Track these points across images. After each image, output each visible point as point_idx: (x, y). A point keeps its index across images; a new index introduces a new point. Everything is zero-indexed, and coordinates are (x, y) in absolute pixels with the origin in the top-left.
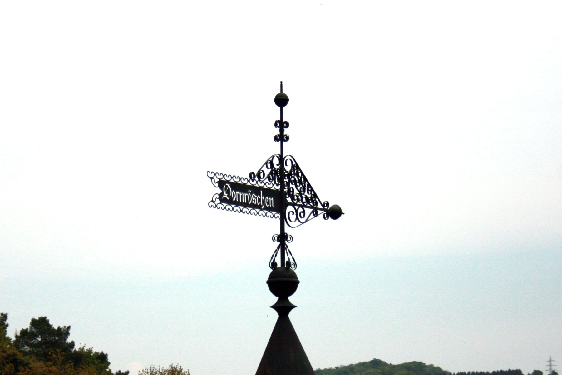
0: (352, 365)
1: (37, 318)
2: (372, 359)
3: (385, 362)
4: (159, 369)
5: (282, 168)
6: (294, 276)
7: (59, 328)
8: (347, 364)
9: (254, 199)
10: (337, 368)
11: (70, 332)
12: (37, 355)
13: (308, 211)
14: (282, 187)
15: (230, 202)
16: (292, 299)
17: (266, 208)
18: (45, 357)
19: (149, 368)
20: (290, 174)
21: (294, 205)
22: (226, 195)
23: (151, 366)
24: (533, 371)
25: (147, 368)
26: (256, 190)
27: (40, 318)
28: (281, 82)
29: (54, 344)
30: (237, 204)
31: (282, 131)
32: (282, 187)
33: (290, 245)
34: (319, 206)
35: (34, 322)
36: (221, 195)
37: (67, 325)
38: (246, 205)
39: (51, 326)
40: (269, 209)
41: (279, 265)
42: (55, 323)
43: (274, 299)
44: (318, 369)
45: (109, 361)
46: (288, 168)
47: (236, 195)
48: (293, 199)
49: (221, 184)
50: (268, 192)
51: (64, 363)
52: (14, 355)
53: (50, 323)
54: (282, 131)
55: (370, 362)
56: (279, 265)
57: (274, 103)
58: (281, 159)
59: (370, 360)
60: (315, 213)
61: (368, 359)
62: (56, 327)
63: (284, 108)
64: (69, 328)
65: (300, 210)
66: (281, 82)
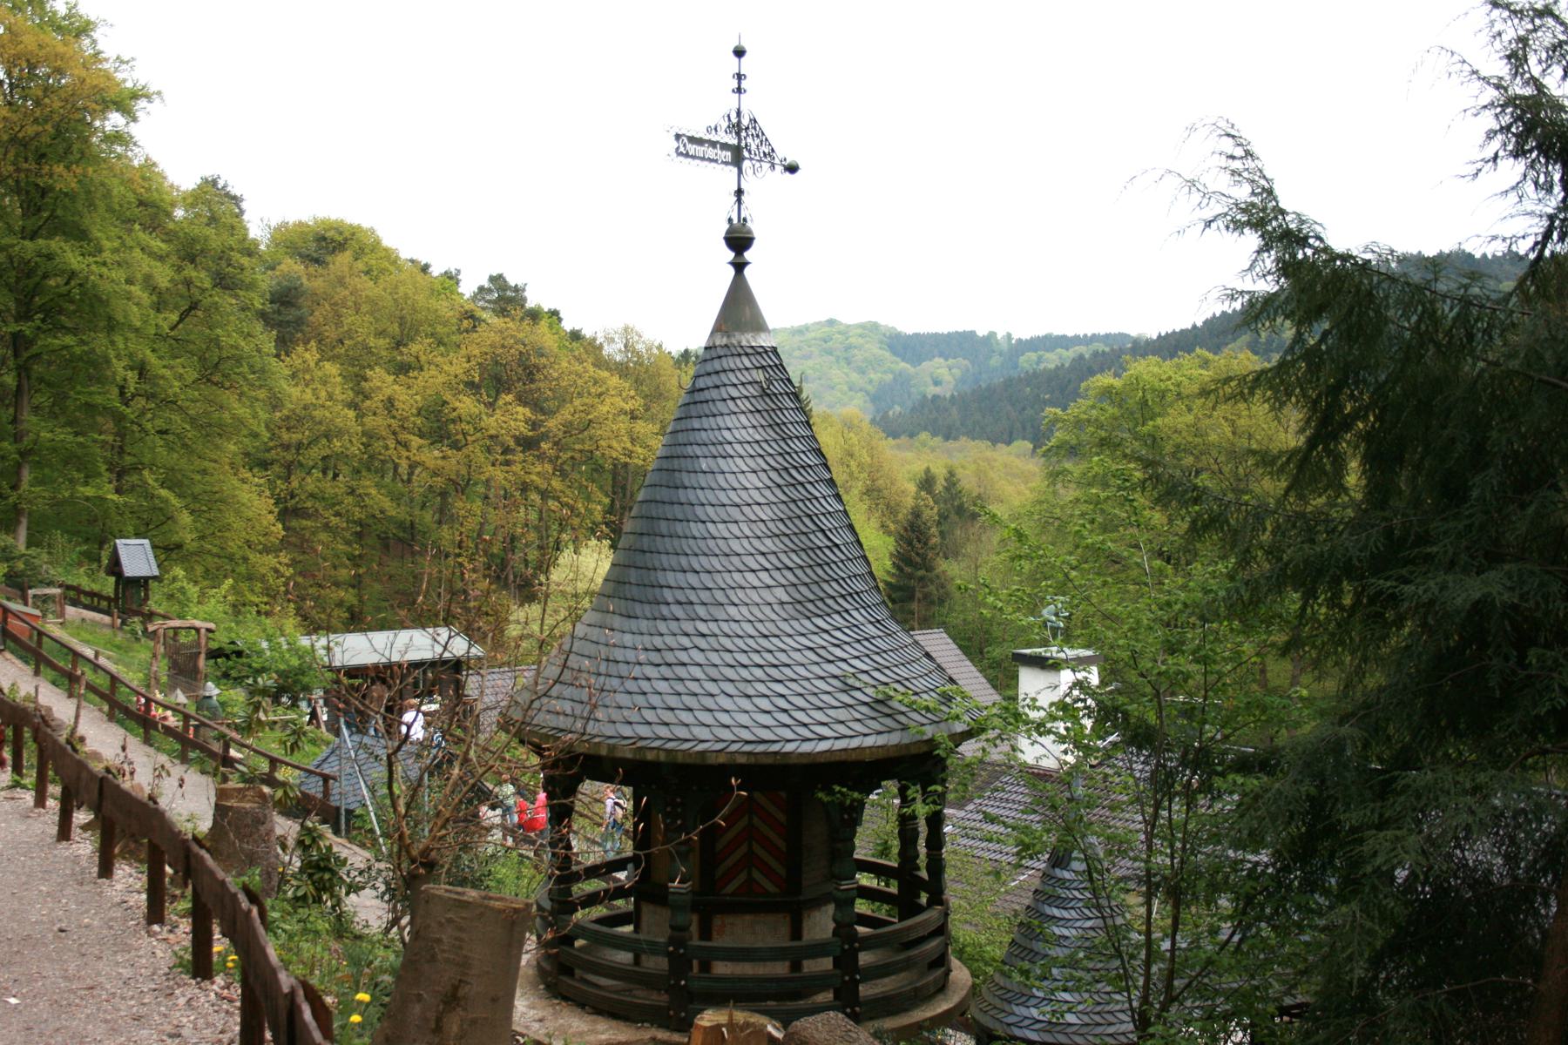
0: (973, 333)
5: (739, 122)
6: (750, 232)
9: (711, 153)
12: (494, 310)
13: (766, 166)
14: (740, 140)
15: (687, 155)
16: (748, 255)
17: (723, 162)
18: (502, 312)
20: (747, 128)
21: (751, 159)
22: (682, 149)
24: (986, 334)
26: (713, 144)
29: (510, 300)
30: (693, 157)
31: (739, 84)
32: (740, 140)
33: (743, 198)
34: (777, 161)
35: (492, 279)
36: (678, 148)
38: (703, 159)
40: (726, 163)
41: (735, 221)
42: (512, 281)
43: (731, 255)
45: (1190, 327)
46: (745, 122)
47: (692, 148)
48: (750, 152)
49: (678, 137)
50: (725, 146)
51: (522, 319)
52: (472, 311)
54: (739, 84)
56: (735, 221)
57: (723, 242)
58: (739, 113)
60: (773, 166)
61: (824, 318)
63: (727, 226)
65: (758, 165)
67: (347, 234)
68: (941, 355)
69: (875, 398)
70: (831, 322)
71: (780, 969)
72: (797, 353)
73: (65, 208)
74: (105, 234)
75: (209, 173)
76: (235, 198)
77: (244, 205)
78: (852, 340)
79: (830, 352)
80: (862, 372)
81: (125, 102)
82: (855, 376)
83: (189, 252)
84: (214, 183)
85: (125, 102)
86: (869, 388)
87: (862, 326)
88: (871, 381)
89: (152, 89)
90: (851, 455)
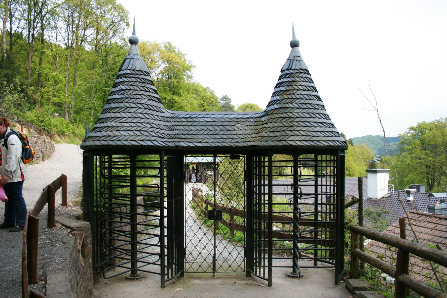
61: (368, 135)
67: (251, 106)
68: (393, 141)
69: (379, 151)
70: (370, 135)
71: (262, 192)
72: (363, 142)
73: (177, 89)
74: (185, 95)
75: (224, 95)
76: (229, 99)
77: (231, 100)
78: (374, 139)
79: (369, 141)
80: (376, 145)
81: (189, 68)
82: (375, 146)
83: (204, 98)
84: (225, 96)
85: (189, 68)
86: (378, 148)
87: (376, 136)
88: (378, 147)
89: (194, 65)
90: (363, 153)
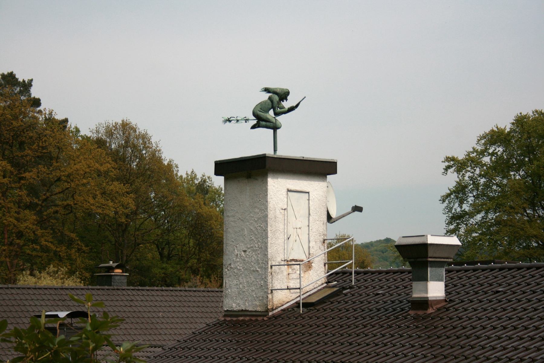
0: (372, 242)
1: (6, 73)
2: (385, 238)
3: (394, 240)
4: (112, 123)
7: (24, 81)
8: (368, 241)
10: (362, 244)
11: (32, 83)
19: (105, 123)
23: (106, 121)
25: (102, 123)
27: (8, 73)
28: (305, 97)
37: (30, 79)
39: (17, 79)
42: (21, 77)
44: (275, 174)
53: (17, 77)
55: (384, 240)
59: (384, 239)
61: (383, 238)
62: (21, 80)
64: (32, 80)
66: (305, 97)
